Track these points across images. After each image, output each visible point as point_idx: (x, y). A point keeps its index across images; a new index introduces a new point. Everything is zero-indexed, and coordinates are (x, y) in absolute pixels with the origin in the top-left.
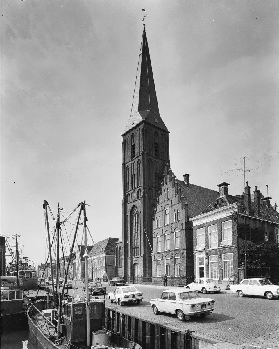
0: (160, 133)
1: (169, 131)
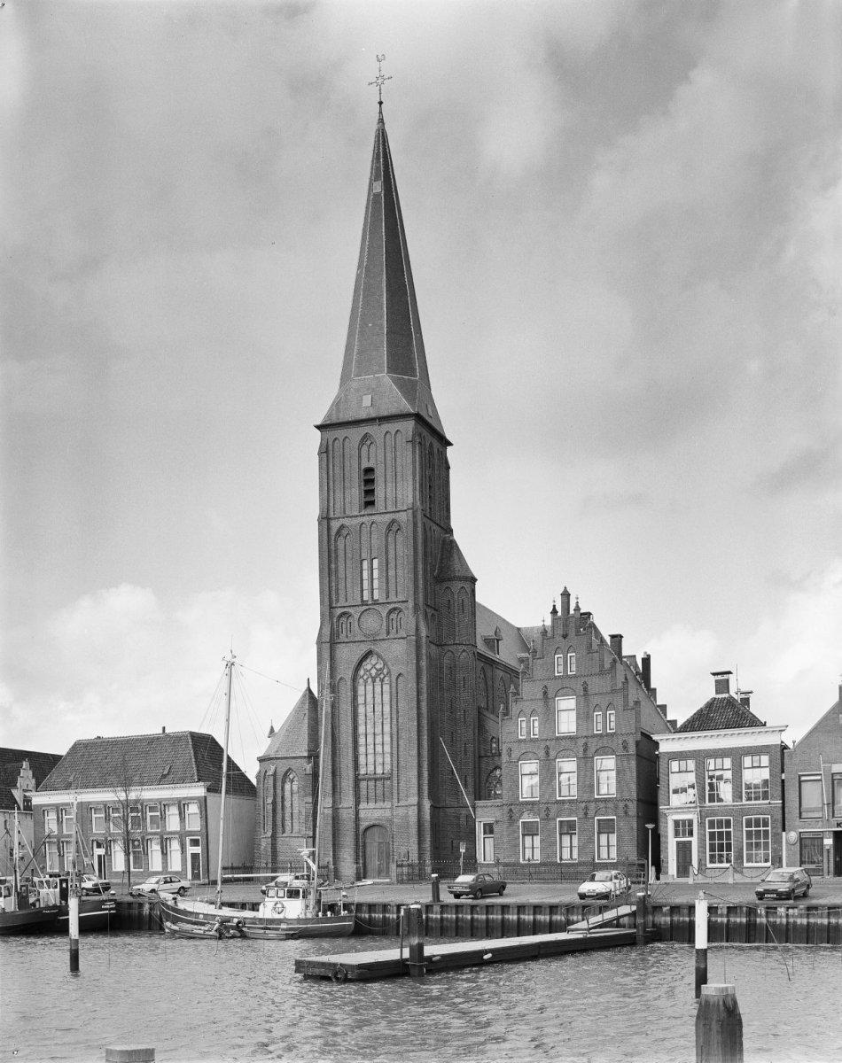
0: (436, 445)
1: (449, 437)
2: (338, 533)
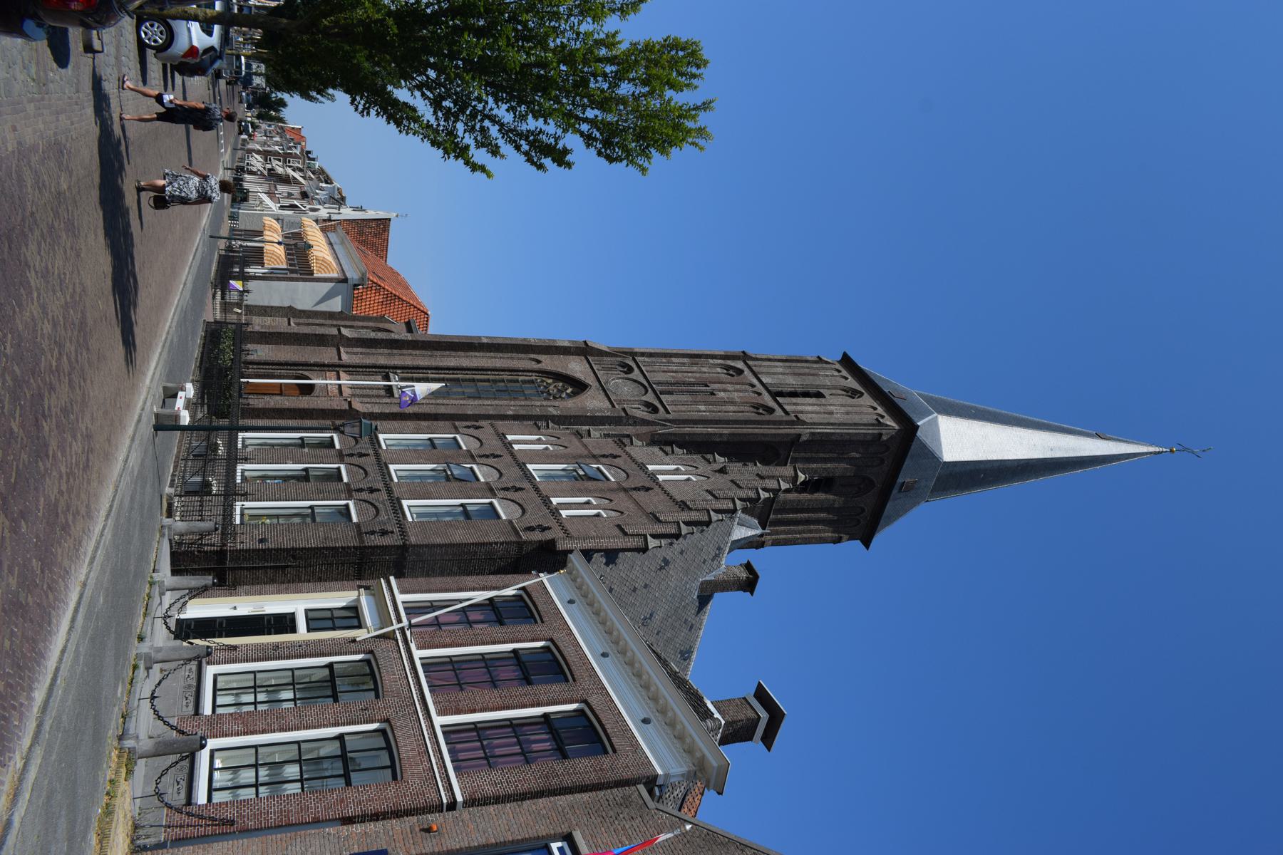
2: (728, 368)
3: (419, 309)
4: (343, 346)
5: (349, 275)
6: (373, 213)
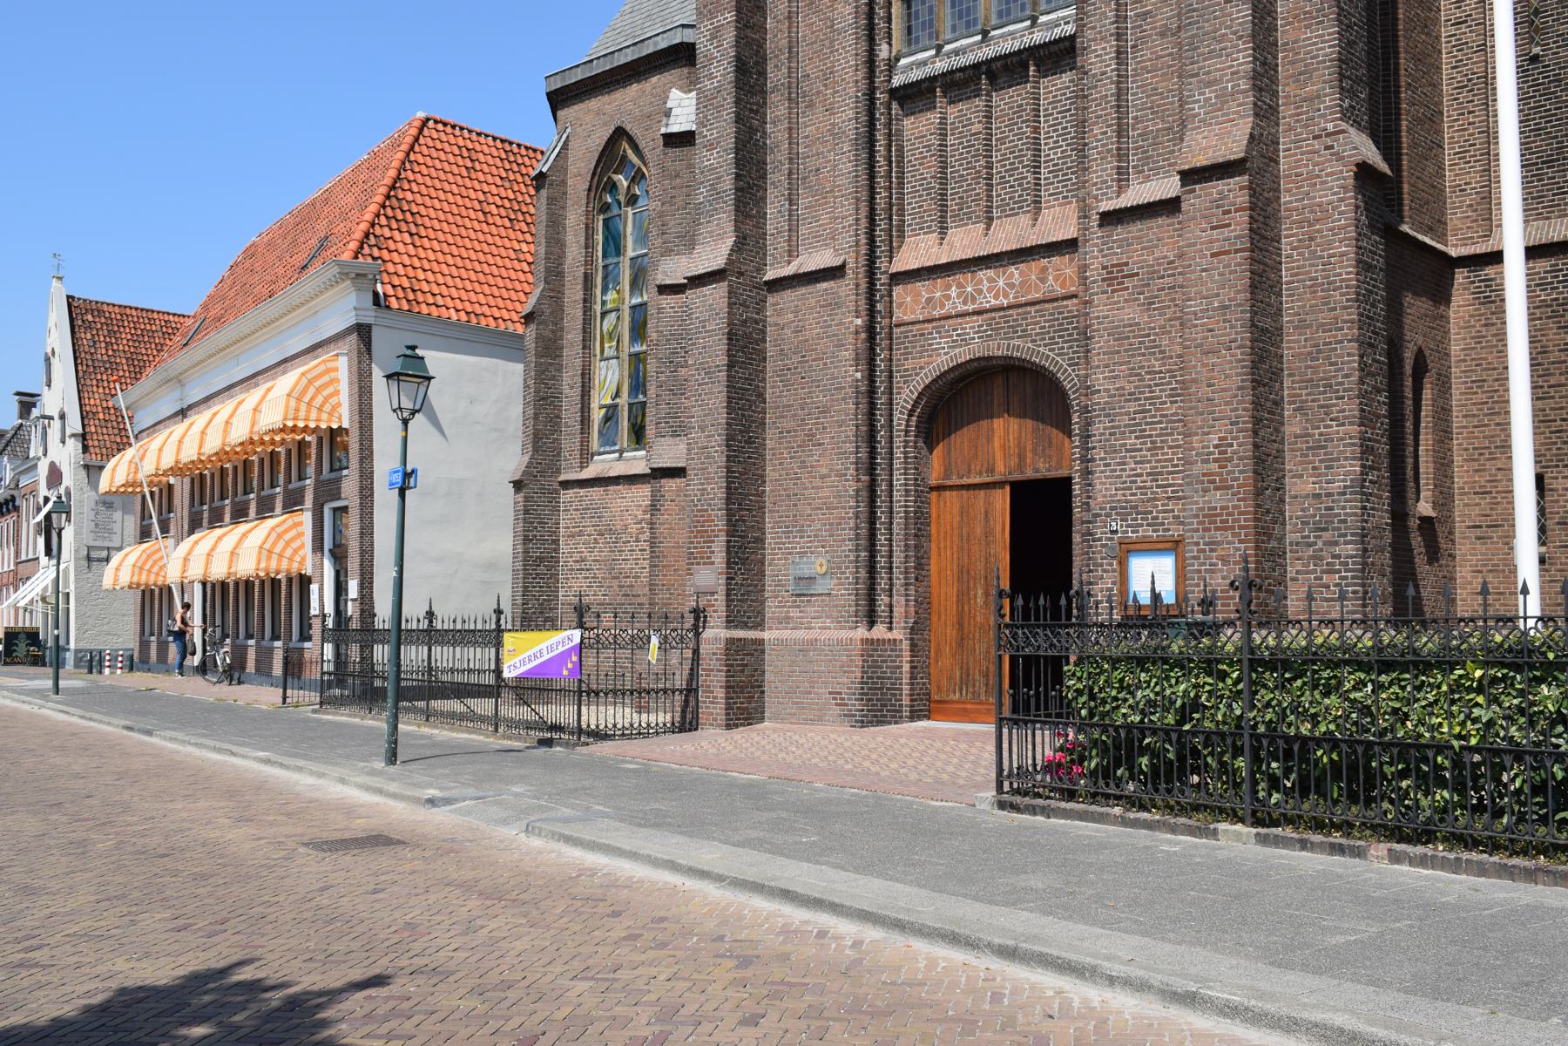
3: (417, 140)
4: (760, 269)
5: (350, 320)
6: (54, 334)
